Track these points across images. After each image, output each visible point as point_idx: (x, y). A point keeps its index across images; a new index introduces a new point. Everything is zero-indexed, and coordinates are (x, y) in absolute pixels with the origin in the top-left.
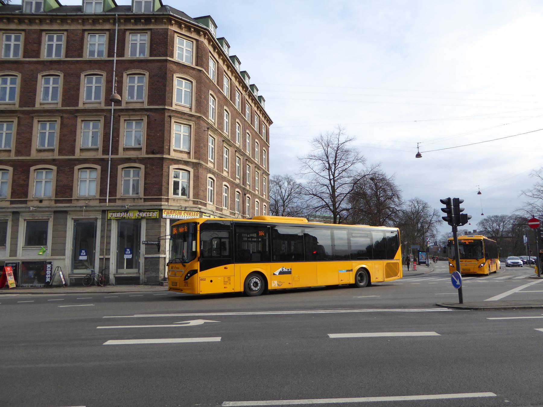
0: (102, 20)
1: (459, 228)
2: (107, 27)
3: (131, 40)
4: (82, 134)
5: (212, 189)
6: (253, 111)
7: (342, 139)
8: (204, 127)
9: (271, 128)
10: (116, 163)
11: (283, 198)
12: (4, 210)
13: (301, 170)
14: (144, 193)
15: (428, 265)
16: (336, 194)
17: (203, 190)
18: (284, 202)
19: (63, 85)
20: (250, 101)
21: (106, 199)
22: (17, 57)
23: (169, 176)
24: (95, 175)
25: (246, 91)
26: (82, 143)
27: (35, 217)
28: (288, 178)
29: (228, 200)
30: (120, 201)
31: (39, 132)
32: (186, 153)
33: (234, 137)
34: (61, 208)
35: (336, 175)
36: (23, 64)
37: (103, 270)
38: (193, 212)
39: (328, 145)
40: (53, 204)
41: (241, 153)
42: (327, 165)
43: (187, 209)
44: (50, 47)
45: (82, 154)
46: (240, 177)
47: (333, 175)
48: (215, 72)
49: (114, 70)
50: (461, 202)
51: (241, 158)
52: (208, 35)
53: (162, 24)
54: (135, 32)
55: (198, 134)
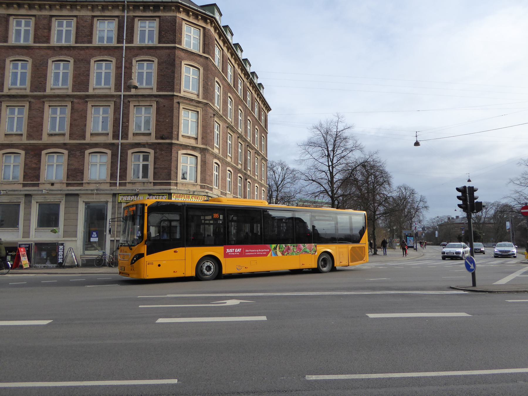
1: (473, 216)
3: (140, 27)
4: (92, 119)
5: (217, 174)
6: (253, 98)
7: (341, 127)
8: (211, 113)
9: (270, 115)
10: (126, 147)
11: (277, 184)
12: (16, 193)
13: (301, 156)
14: (154, 178)
15: (416, 249)
16: (335, 180)
17: (209, 175)
18: (277, 187)
19: (73, 71)
20: (251, 88)
21: (117, 183)
22: (27, 42)
23: (178, 161)
24: (106, 159)
25: (247, 79)
26: (92, 128)
28: (282, 164)
29: (231, 185)
30: (131, 185)
31: (50, 117)
32: (193, 138)
33: (236, 123)
35: (334, 162)
36: (34, 50)
37: (114, 252)
38: (201, 196)
39: (328, 133)
40: (64, 187)
41: (243, 139)
42: (326, 152)
43: (195, 194)
44: (60, 32)
45: (92, 139)
46: (242, 163)
47: (332, 162)
48: (220, 59)
49: (124, 56)
50: (476, 191)
51: (243, 144)
52: (214, 23)
53: (171, 12)
55: (205, 120)
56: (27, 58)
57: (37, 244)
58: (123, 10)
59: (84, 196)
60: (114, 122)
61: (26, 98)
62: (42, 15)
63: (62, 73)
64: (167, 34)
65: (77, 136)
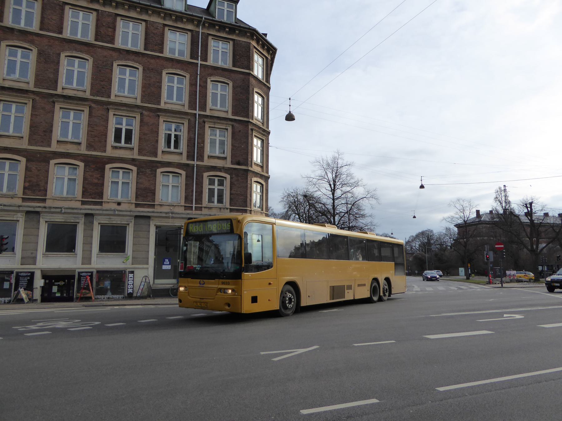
0: (164, 14)
2: (190, 27)
12: (75, 211)
19: (142, 80)
27: (113, 221)
30: (206, 210)
34: (145, 213)
45: (163, 157)
54: (217, 39)
56: (86, 56)
57: (98, 272)
58: (198, 26)
59: (157, 219)
60: (189, 141)
61: (86, 102)
62: (106, 11)
63: (77, 71)
64: (241, 58)
65: (147, 151)
